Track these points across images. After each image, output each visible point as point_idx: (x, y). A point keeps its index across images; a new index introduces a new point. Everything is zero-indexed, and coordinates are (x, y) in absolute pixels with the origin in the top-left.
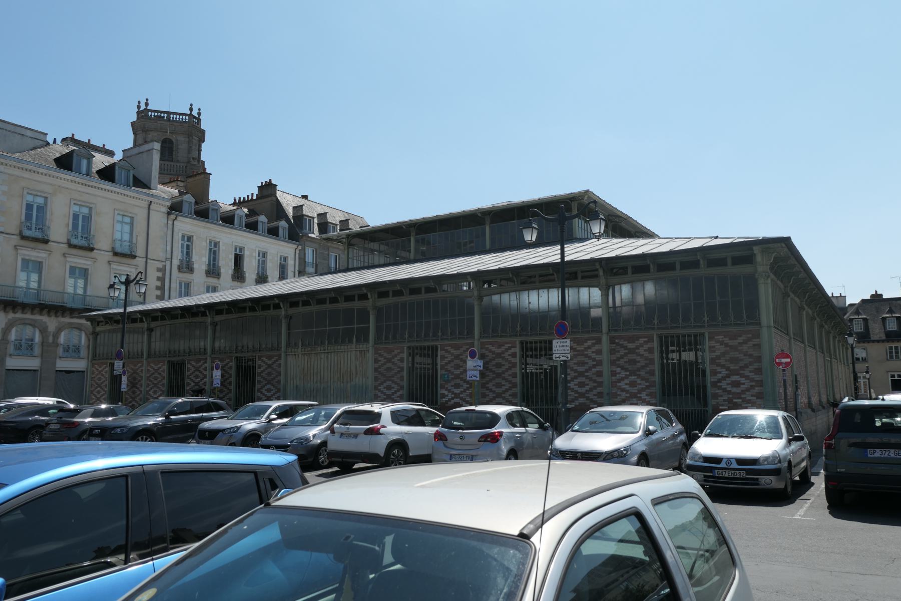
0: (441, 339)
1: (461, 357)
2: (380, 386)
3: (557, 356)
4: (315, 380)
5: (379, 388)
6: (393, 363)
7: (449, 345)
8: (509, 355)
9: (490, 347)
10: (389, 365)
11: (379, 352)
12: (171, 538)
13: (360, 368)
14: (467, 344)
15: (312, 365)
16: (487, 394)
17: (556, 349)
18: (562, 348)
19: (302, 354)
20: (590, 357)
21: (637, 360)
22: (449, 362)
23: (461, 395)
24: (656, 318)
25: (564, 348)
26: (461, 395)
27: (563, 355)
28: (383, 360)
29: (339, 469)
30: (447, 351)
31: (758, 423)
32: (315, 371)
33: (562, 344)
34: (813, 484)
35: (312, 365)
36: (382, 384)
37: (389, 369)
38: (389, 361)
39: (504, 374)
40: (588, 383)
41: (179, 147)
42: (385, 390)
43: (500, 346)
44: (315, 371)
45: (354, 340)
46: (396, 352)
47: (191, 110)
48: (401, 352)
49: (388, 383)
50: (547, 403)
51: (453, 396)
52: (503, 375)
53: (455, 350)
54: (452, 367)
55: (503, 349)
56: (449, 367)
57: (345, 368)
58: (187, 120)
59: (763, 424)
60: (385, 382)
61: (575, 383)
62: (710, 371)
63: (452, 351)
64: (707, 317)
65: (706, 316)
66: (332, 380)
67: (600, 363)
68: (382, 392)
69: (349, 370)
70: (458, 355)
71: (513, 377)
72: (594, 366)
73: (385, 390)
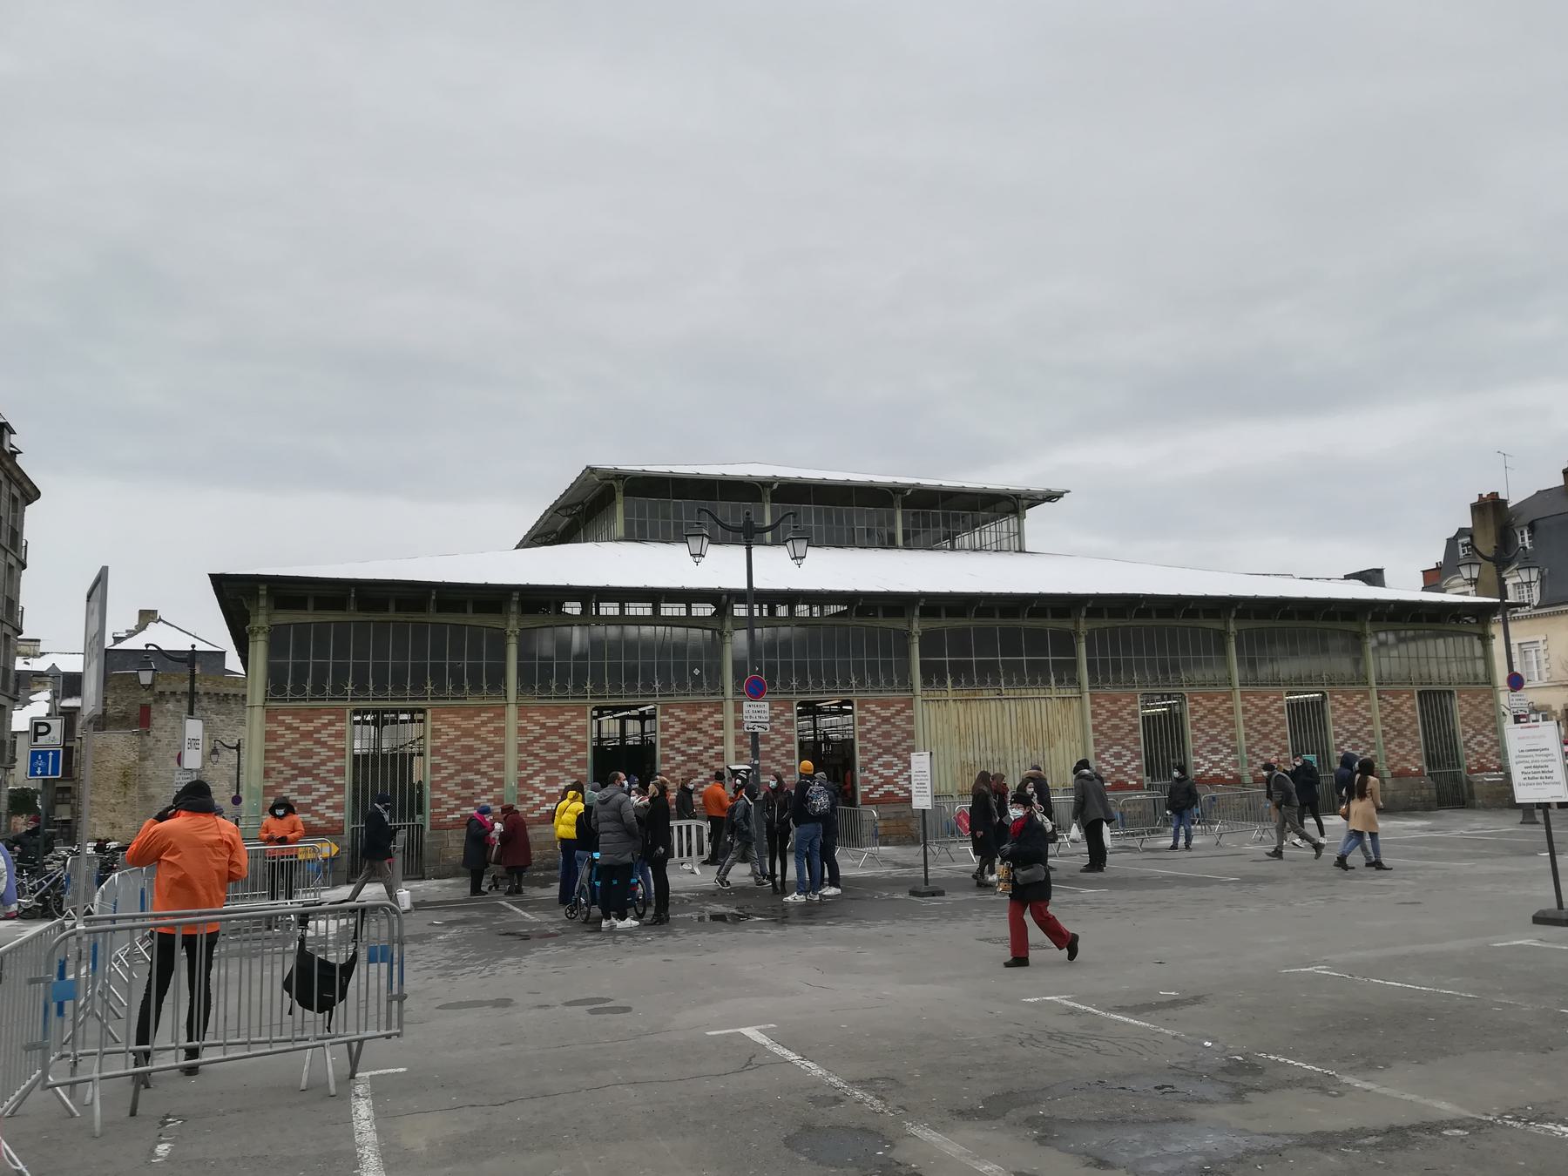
1: (1217, 711)
3: (751, 726)
4: (982, 746)
5: (1103, 756)
6: (1122, 719)
7: (1199, 694)
8: (1275, 710)
10: (1115, 721)
11: (1098, 700)
13: (1064, 726)
14: (1223, 694)
15: (975, 722)
16: (1254, 761)
17: (748, 715)
18: (758, 714)
19: (954, 700)
20: (484, 740)
22: (1202, 718)
23: (1222, 764)
24: (588, 683)
25: (760, 714)
26: (1222, 764)
27: (759, 724)
28: (1105, 715)
29: (1028, 908)
30: (1196, 702)
31: (1356, 796)
32: (982, 730)
33: (757, 709)
35: (975, 722)
36: (1107, 749)
37: (1116, 728)
38: (1114, 714)
39: (1272, 734)
40: (702, 771)
42: (1112, 760)
43: (1264, 698)
44: (982, 730)
45: (1053, 680)
46: (1124, 701)
48: (1131, 703)
49: (1116, 749)
50: (1439, 766)
51: (1211, 765)
52: (1271, 736)
53: (1208, 701)
54: (1205, 725)
55: (1267, 701)
56: (1201, 725)
57: (1039, 726)
59: (1359, 798)
60: (1111, 746)
61: (702, 776)
62: (431, 767)
63: (1204, 702)
64: (352, 686)
65: (429, 684)
66: (1015, 746)
67: (720, 741)
68: (1108, 763)
69: (1045, 728)
70: (1213, 709)
71: (1282, 739)
72: (1365, 725)
73: (1112, 760)
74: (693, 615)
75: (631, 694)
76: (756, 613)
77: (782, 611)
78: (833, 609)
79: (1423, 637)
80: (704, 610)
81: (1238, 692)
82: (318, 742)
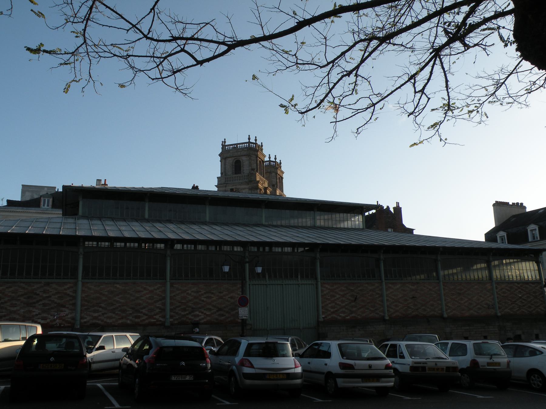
0: (152, 279)
2: (339, 297)
9: (327, 286)
12: (486, 23)
18: (243, 312)
21: (200, 315)
34: (64, 187)
41: (244, 164)
45: (299, 276)
47: (249, 139)
58: (247, 146)
74: (273, 251)
75: (58, 277)
76: (296, 251)
77: (267, 249)
78: (301, 249)
79: (517, 262)
80: (288, 249)
81: (384, 283)
82: (188, 294)
